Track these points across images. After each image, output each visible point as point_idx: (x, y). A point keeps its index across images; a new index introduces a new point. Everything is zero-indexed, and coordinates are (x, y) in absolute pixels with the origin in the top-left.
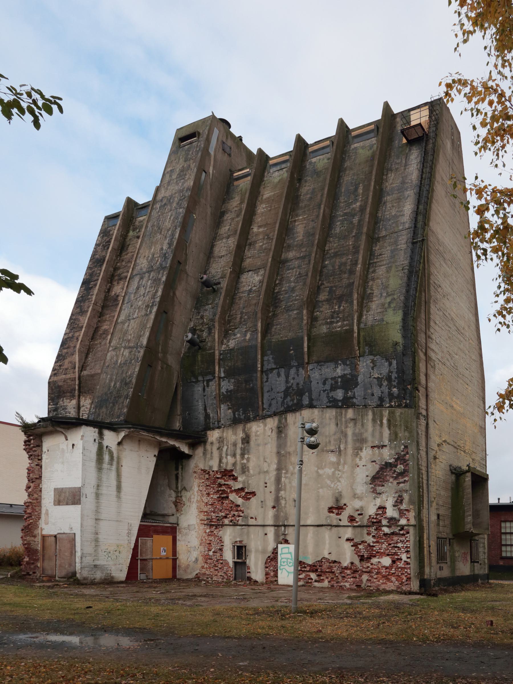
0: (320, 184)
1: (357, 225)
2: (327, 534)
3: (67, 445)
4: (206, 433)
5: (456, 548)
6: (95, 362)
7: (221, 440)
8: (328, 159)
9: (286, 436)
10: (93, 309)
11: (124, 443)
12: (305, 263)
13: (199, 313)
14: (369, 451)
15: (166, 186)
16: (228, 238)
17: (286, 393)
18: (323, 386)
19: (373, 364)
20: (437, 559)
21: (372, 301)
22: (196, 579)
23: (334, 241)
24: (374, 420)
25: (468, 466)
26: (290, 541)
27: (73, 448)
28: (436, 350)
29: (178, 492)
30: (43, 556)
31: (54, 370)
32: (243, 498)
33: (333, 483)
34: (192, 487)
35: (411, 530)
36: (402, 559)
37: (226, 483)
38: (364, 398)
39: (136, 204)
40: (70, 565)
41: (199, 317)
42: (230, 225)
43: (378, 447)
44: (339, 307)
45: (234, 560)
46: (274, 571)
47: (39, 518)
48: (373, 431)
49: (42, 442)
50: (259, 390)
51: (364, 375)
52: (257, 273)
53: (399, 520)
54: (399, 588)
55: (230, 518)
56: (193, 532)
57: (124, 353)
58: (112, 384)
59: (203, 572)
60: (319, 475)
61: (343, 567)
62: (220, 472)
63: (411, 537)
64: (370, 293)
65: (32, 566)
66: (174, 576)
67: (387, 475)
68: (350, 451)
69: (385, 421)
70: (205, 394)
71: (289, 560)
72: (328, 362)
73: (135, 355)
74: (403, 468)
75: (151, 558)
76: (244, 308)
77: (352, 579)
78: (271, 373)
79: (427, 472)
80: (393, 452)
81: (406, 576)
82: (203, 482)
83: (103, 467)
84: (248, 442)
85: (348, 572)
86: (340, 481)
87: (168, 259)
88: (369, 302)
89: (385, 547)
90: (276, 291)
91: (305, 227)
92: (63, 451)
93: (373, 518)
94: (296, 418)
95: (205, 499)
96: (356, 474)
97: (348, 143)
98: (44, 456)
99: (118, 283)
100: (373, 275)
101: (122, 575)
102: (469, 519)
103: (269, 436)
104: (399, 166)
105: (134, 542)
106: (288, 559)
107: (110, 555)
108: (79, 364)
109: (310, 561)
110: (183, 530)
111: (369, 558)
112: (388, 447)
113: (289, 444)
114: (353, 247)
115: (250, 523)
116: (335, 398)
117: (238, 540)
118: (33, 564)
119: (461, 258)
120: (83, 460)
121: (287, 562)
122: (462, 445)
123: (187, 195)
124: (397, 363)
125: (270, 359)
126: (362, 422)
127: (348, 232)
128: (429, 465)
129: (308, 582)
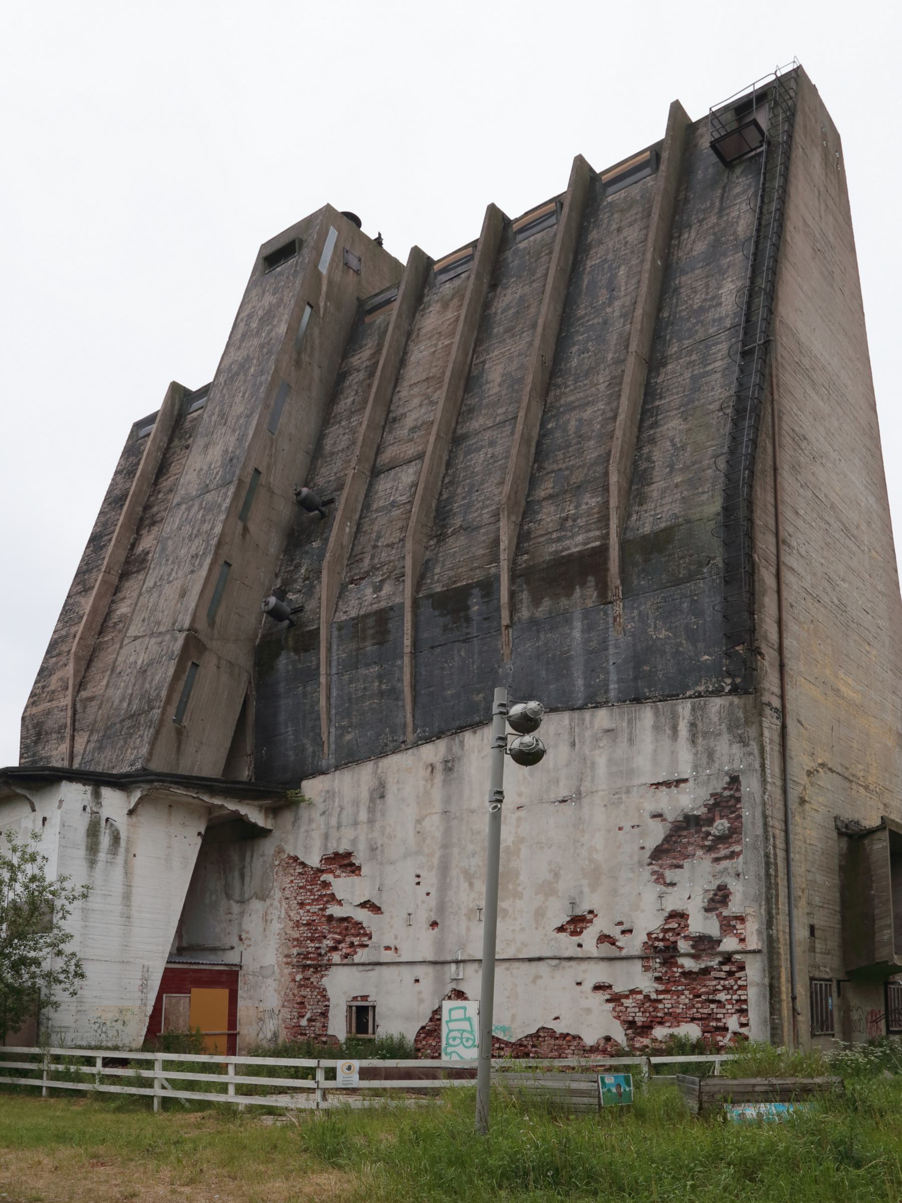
3: (34, 821)
5: (854, 1001)
10: (104, 582)
13: (292, 560)
20: (813, 1028)
23: (565, 384)
24: (656, 728)
25: (553, 977)
26: (469, 994)
27: (44, 824)
28: (800, 570)
31: (33, 695)
36: (726, 1029)
42: (356, 394)
53: (721, 941)
56: (270, 981)
64: (645, 470)
67: (689, 843)
71: (466, 1035)
79: (786, 832)
83: (98, 859)
88: (643, 486)
89: (687, 1001)
93: (657, 939)
94: (482, 739)
99: (149, 531)
105: (153, 1003)
106: (464, 1031)
119: (849, 382)
120: (60, 845)
121: (461, 1039)
122: (861, 774)
128: (790, 816)
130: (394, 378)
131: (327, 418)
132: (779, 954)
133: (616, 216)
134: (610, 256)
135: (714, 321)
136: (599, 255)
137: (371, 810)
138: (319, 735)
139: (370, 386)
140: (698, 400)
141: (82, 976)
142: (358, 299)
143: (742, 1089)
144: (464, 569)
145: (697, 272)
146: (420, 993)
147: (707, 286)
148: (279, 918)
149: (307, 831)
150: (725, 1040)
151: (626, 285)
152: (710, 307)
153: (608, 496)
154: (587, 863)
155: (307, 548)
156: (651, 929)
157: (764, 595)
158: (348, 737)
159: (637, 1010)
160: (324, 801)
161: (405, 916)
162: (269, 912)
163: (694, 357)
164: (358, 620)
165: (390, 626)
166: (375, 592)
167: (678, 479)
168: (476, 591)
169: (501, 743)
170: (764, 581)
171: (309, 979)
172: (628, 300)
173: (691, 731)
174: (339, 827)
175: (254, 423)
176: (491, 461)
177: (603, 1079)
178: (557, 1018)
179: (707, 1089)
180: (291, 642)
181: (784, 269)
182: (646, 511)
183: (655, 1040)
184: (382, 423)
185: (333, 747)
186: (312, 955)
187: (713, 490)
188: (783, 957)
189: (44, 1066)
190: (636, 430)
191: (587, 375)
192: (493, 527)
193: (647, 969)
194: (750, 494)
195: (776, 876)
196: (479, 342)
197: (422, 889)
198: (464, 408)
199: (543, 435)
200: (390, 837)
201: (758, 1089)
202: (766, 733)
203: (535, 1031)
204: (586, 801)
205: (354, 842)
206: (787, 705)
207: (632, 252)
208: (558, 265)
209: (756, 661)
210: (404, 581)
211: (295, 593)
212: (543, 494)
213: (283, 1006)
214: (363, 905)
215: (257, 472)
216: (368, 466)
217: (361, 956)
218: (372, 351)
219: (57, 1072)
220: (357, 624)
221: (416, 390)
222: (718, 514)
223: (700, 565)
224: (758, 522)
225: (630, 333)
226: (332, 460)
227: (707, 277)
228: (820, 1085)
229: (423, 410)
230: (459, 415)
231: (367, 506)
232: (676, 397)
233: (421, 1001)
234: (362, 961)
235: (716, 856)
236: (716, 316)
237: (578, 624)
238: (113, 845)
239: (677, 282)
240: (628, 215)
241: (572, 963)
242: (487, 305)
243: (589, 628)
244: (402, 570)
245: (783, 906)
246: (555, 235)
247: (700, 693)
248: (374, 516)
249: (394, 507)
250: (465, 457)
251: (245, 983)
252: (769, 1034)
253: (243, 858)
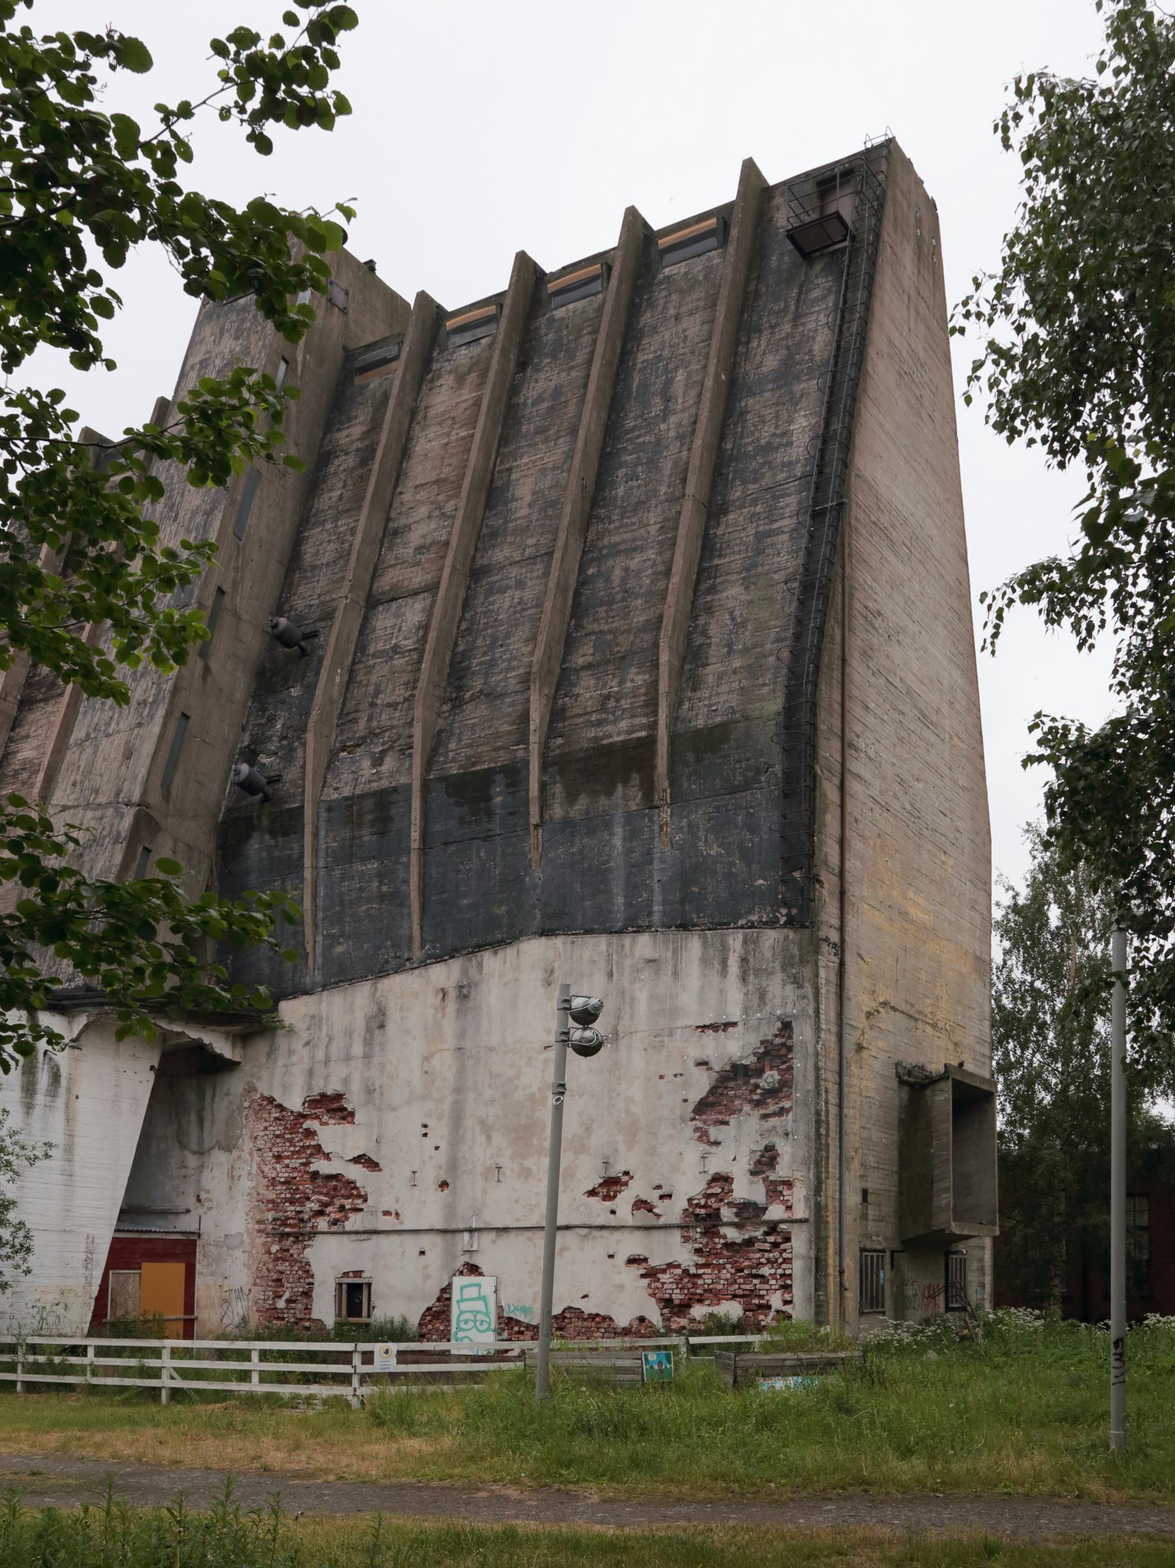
5: (909, 1274)
12: (535, 574)
13: (264, 710)
21: (705, 665)
23: (609, 517)
24: (705, 961)
25: (582, 1249)
26: (484, 1268)
36: (769, 1307)
41: (264, 721)
42: (344, 487)
53: (766, 1209)
56: (238, 1253)
64: (701, 646)
71: (480, 1317)
79: (840, 1084)
83: (35, 1102)
88: (697, 667)
89: (729, 1276)
93: (698, 1206)
102: (945, 1199)
105: (99, 1281)
106: (478, 1312)
121: (475, 1321)
122: (929, 1010)
130: (394, 473)
131: (304, 519)
132: (827, 1222)
133: (674, 297)
134: (666, 353)
135: (783, 464)
136: (652, 349)
137: (368, 1042)
138: (302, 944)
139: (364, 479)
140: (762, 565)
141: (28, 1250)
142: (344, 348)
143: (773, 1364)
144: (485, 749)
145: (766, 395)
146: (426, 1267)
147: (777, 416)
148: (250, 1174)
149: (285, 1066)
150: (767, 1320)
151: (684, 396)
152: (780, 445)
153: (658, 675)
154: (623, 1116)
155: (283, 695)
156: (692, 1194)
157: (825, 813)
158: (339, 949)
159: (674, 1286)
160: (308, 1029)
161: (410, 1174)
162: (236, 1166)
163: (759, 509)
164: (351, 800)
165: (393, 812)
166: (374, 766)
167: (737, 664)
168: (499, 778)
169: (564, 1038)
170: (825, 795)
171: (287, 1250)
172: (685, 418)
173: (742, 967)
174: (327, 1062)
175: (217, 524)
176: (519, 608)
177: (646, 1356)
178: (585, 1296)
179: (741, 1364)
180: (265, 822)
181: (863, 410)
182: (700, 699)
183: (693, 1320)
184: (381, 534)
185: (320, 960)
186: (291, 1221)
187: (775, 683)
188: (831, 1226)
189: (20, 1358)
190: (691, 593)
191: (635, 511)
192: (519, 697)
193: (686, 1239)
194: (814, 694)
195: (827, 1136)
196: (504, 441)
197: (429, 1143)
198: (485, 531)
199: (582, 583)
200: (391, 1077)
201: (787, 1363)
202: (822, 973)
203: (560, 1312)
204: (623, 1043)
205: (346, 1081)
206: (847, 938)
207: (693, 352)
208: (603, 357)
209: (814, 890)
210: (410, 755)
211: (269, 755)
212: (581, 661)
213: (255, 1284)
214: (357, 1160)
215: (221, 591)
216: (362, 593)
217: (354, 1222)
218: (365, 429)
219: (36, 1363)
220: (351, 806)
221: (423, 495)
222: (779, 714)
223: (758, 772)
224: (823, 727)
225: (687, 463)
226: (314, 576)
227: (777, 404)
228: (843, 1359)
229: (433, 525)
230: (478, 539)
231: (361, 647)
232: (737, 557)
233: (427, 1277)
234: (354, 1229)
235: (764, 1112)
236: (786, 459)
237: (619, 830)
238: (52, 1085)
239: (743, 404)
240: (688, 299)
241: (605, 1233)
242: (514, 390)
243: (631, 836)
244: (408, 740)
245: (833, 1169)
246: (601, 308)
247: (753, 923)
248: (372, 662)
249: (397, 653)
250: (486, 597)
251: (205, 1256)
252: (813, 1312)
253: (201, 1097)
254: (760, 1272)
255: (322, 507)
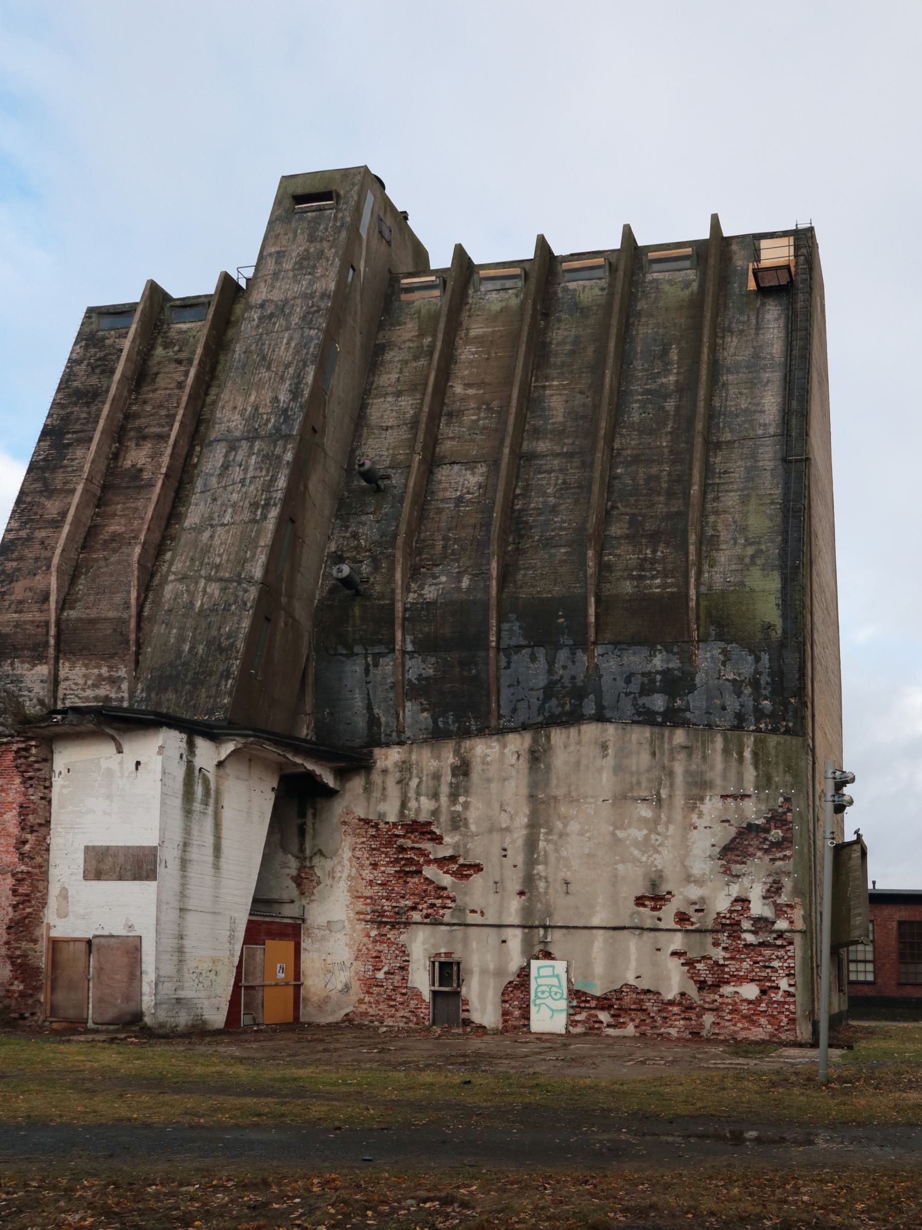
0: (589, 331)
1: (675, 415)
2: (633, 944)
4: (371, 752)
6: (97, 594)
7: (405, 767)
8: (602, 289)
9: (548, 767)
10: (85, 490)
11: (227, 764)
12: (575, 465)
13: (347, 527)
14: (719, 803)
15: (269, 281)
16: (398, 396)
17: (549, 691)
18: (624, 685)
19: (725, 656)
21: (718, 550)
22: (347, 1023)
24: (726, 751)
27: (137, 769)
29: (305, 858)
30: (54, 981)
32: (454, 874)
33: (646, 855)
34: (337, 850)
35: (798, 939)
36: (779, 988)
37: (416, 845)
38: (707, 713)
39: (166, 297)
40: (127, 998)
41: (348, 535)
42: (401, 372)
43: (735, 797)
44: (654, 552)
45: (433, 988)
46: (520, 1008)
47: (44, 904)
48: (725, 769)
49: (52, 752)
50: (492, 681)
51: (706, 673)
52: (472, 469)
54: (775, 1036)
55: (425, 912)
56: (339, 936)
57: (208, 590)
58: (187, 648)
59: (360, 1010)
60: (617, 841)
61: (666, 1001)
62: (402, 825)
63: (797, 949)
64: (712, 536)
65: (30, 1001)
66: (296, 1018)
67: (749, 845)
68: (680, 800)
69: (747, 754)
70: (368, 679)
71: (554, 989)
72: (635, 644)
73: (237, 596)
74: (781, 834)
75: (262, 983)
76: (449, 530)
77: (682, 1022)
78: (516, 653)
80: (763, 808)
81: (787, 1016)
82: (363, 843)
83: (194, 808)
84: (466, 774)
85: (676, 1009)
86: (658, 852)
87: (294, 420)
89: (748, 966)
90: (517, 507)
91: (567, 402)
92: (109, 773)
93: (724, 917)
94: (569, 737)
95: (367, 874)
96: (691, 840)
97: (641, 268)
98: (58, 783)
100: (715, 504)
101: (217, 1018)
103: (512, 766)
104: (745, 328)
106: (552, 986)
107: (201, 979)
108: (58, 595)
109: (597, 989)
110: (317, 931)
111: (716, 986)
112: (754, 799)
113: (554, 782)
114: (671, 451)
115: (469, 921)
116: (649, 709)
117: (443, 950)
118: (31, 996)
120: (162, 793)
121: (550, 992)
123: (322, 305)
124: (770, 659)
125: (514, 628)
126: (704, 752)
127: (657, 424)
129: (593, 1029)
171: (385, 935)
254: (772, 964)
255: (381, 384)
